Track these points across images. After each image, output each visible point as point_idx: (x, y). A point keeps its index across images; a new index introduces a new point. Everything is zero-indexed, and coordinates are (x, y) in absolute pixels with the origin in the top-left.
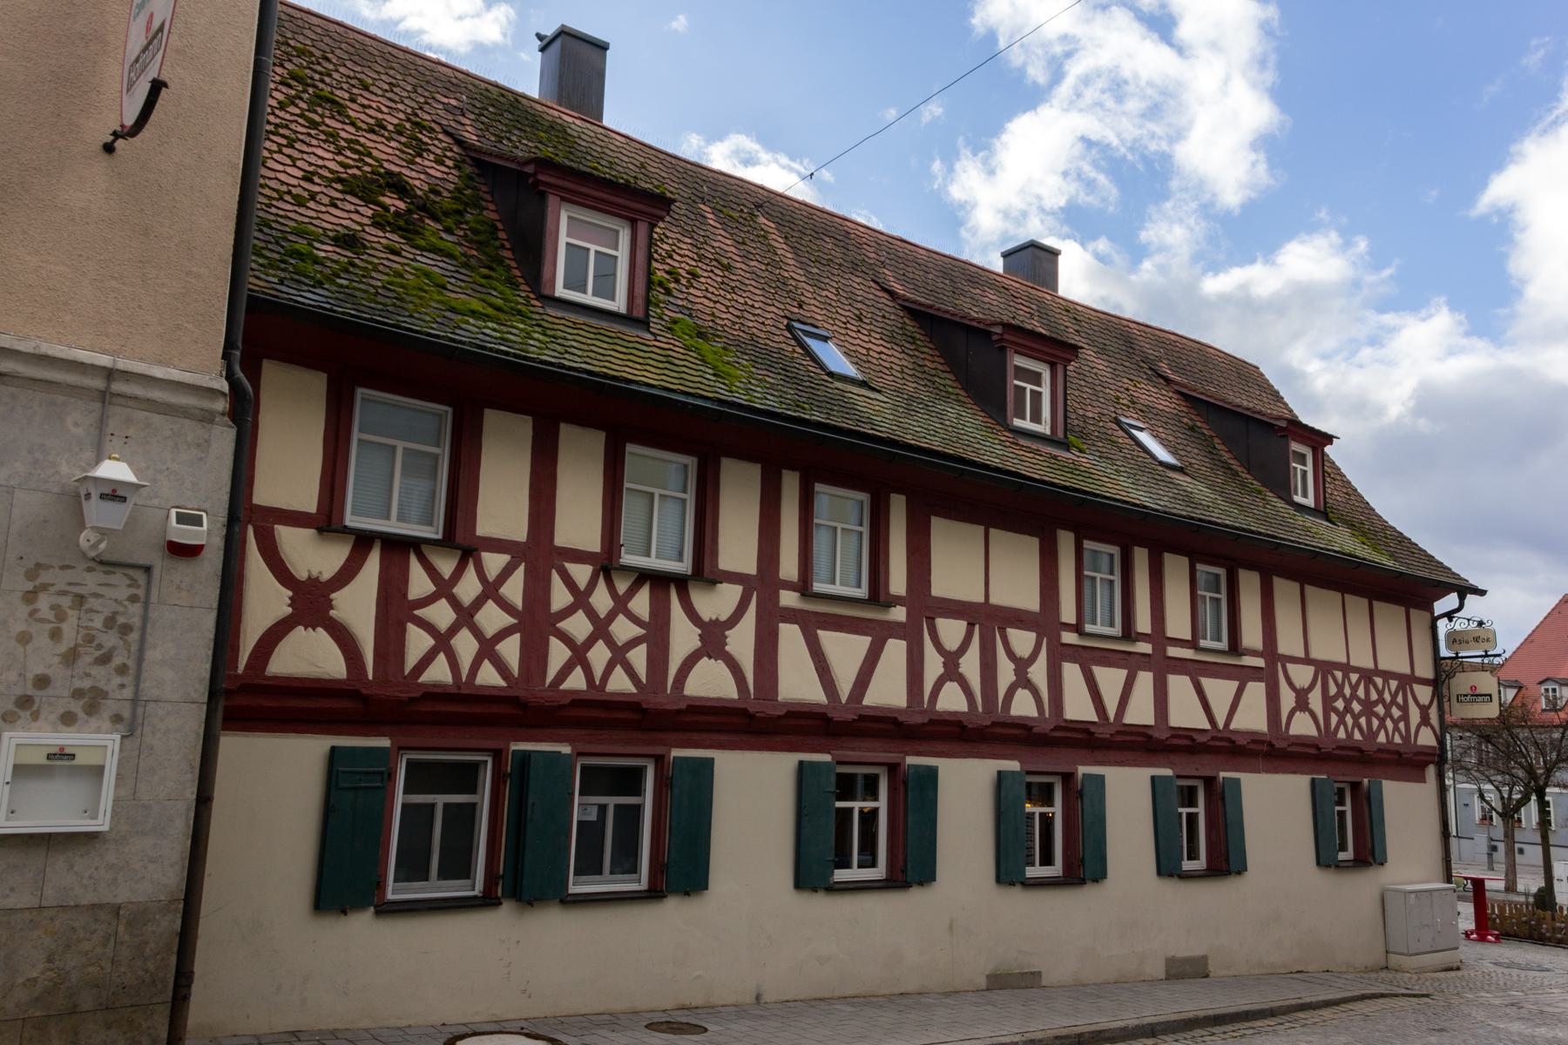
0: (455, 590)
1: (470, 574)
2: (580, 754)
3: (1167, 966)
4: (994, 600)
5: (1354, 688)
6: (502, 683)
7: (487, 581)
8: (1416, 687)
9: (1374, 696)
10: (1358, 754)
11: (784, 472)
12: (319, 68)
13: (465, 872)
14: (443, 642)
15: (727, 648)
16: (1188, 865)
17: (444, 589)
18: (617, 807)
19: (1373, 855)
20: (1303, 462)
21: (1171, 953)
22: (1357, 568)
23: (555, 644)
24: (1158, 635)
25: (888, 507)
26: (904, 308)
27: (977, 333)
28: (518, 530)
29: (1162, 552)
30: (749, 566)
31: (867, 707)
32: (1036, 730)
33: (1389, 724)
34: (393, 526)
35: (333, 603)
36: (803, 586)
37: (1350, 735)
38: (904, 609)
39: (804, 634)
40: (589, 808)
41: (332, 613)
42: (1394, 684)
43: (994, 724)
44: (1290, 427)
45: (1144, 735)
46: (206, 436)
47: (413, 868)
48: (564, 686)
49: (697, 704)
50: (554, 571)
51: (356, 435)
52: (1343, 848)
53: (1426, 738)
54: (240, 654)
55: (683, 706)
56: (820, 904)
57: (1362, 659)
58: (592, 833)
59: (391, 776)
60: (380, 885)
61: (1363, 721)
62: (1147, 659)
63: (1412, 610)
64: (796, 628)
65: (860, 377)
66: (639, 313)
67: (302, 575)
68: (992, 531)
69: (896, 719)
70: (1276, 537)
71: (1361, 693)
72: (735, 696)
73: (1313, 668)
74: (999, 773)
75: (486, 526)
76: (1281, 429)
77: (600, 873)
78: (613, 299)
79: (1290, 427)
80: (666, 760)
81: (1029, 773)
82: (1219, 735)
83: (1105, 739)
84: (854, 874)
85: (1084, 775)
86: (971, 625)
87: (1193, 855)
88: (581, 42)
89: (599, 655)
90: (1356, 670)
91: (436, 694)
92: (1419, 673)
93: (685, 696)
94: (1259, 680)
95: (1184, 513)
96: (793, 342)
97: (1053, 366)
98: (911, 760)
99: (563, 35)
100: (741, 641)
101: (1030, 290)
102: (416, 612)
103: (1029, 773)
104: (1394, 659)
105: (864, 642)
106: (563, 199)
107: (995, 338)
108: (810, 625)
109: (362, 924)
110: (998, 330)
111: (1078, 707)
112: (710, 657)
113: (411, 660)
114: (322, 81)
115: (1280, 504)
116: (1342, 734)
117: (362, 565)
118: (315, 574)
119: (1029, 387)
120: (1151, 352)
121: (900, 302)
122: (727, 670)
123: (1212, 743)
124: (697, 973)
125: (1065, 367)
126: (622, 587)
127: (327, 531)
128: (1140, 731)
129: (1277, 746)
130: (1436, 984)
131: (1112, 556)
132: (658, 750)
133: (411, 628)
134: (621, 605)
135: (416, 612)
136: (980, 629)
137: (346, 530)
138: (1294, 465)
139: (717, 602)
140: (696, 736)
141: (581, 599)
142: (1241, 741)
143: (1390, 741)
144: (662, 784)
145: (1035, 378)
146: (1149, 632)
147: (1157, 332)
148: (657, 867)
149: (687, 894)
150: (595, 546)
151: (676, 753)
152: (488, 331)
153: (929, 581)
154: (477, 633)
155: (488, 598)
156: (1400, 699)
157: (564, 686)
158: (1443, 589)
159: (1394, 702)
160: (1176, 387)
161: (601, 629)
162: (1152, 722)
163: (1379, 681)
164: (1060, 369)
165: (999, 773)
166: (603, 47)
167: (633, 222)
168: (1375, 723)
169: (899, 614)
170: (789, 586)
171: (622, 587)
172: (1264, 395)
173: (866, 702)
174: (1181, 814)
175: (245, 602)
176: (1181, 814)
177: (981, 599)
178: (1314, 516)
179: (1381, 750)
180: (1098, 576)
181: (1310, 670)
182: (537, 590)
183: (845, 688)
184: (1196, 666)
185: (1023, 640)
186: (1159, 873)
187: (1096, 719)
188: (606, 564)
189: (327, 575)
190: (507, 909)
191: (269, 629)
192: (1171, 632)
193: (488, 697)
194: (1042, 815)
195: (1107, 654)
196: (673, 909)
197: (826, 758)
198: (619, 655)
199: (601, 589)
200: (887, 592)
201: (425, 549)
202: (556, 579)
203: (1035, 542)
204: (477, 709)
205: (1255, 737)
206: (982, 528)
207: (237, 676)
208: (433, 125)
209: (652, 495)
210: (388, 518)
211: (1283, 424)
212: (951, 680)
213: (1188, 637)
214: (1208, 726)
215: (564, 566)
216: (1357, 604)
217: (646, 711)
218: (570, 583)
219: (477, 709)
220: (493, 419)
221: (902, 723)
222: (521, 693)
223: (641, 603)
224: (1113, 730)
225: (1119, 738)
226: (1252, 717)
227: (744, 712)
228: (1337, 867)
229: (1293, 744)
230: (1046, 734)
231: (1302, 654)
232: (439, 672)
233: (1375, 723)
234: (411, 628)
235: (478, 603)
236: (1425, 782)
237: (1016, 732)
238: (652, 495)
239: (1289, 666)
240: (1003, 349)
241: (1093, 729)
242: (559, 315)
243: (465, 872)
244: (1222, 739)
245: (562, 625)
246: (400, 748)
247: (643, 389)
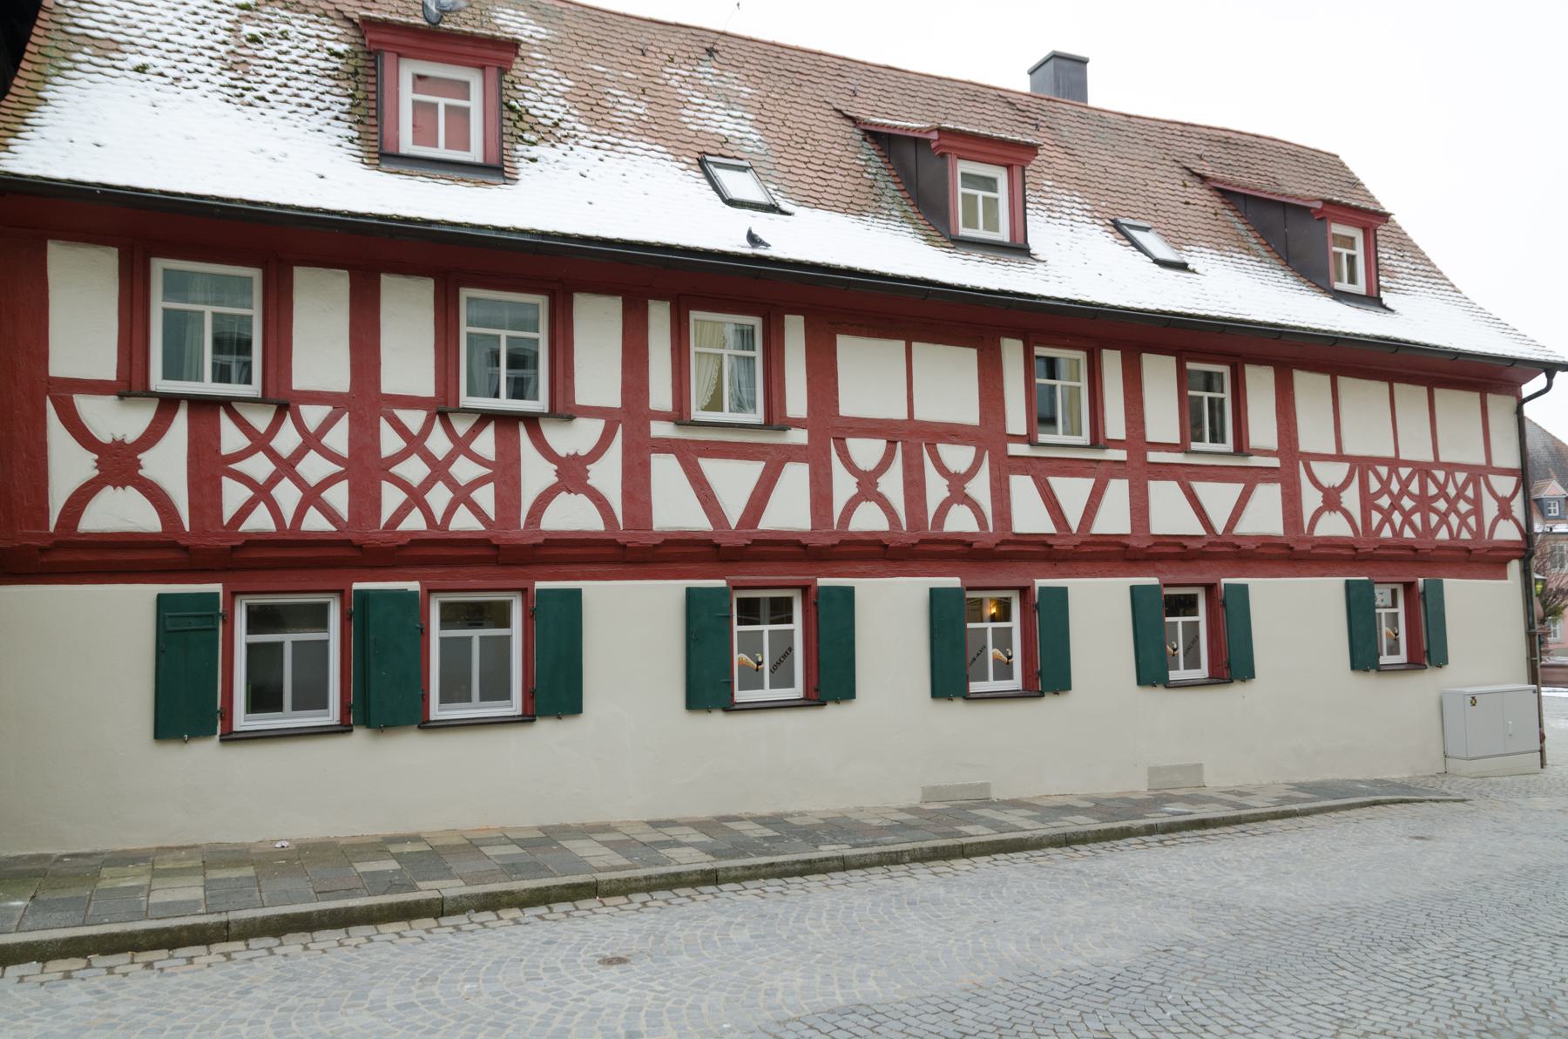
0: (272, 444)
1: (288, 426)
2: (736, 588)
6: (332, 528)
8: (1493, 478)
10: (1411, 553)
11: (650, 302)
13: (505, 694)
15: (589, 482)
17: (260, 443)
18: (482, 638)
22: (1279, 337)
24: (1136, 438)
27: (917, 142)
28: (338, 379)
30: (613, 399)
31: (763, 531)
35: (141, 463)
36: (680, 416)
37: (1397, 533)
41: (141, 472)
43: (922, 541)
44: (1326, 209)
47: (455, 691)
49: (594, 537)
50: (382, 419)
51: (693, 349)
53: (1507, 532)
54: (51, 514)
55: (540, 540)
56: (1157, 695)
60: (227, 715)
62: (1122, 467)
63: (1395, 384)
66: (493, 161)
68: (915, 345)
71: (1414, 487)
74: (932, 590)
75: (301, 380)
76: (1319, 211)
77: (469, 699)
78: (467, 148)
80: (529, 593)
82: (1218, 541)
85: (1040, 588)
86: (892, 443)
89: (439, 497)
90: (1407, 463)
91: (258, 541)
92: (1498, 462)
93: (541, 531)
98: (823, 582)
105: (1236, 489)
107: (933, 145)
108: (689, 455)
109: (206, 751)
111: (1030, 517)
113: (229, 511)
116: (1387, 533)
117: (169, 426)
118: (119, 437)
119: (981, 194)
121: (863, 127)
123: (1208, 549)
126: (462, 427)
127: (128, 396)
132: (521, 583)
133: (226, 481)
134: (462, 446)
136: (990, 456)
138: (1335, 249)
140: (564, 569)
141: (415, 444)
143: (1397, 533)
144: (529, 616)
148: (528, 695)
155: (310, 449)
156: (1470, 492)
162: (1128, 531)
163: (1440, 475)
165: (932, 590)
168: (1434, 519)
170: (661, 416)
171: (462, 427)
177: (904, 415)
179: (1441, 547)
180: (725, 352)
182: (365, 439)
183: (1074, 521)
185: (958, 457)
188: (442, 409)
190: (360, 736)
191: (77, 490)
193: (317, 542)
195: (1066, 464)
198: (462, 495)
199: (438, 433)
201: (236, 406)
203: (972, 353)
204: (590, 551)
205: (1266, 542)
207: (51, 535)
210: (497, 395)
211: (1319, 205)
212: (867, 500)
213: (1177, 440)
214: (1201, 531)
217: (497, 546)
219: (590, 551)
221: (806, 546)
222: (352, 535)
223: (486, 443)
224: (1078, 541)
227: (612, 543)
228: (1379, 670)
229: (1319, 546)
230: (991, 549)
231: (1333, 451)
232: (260, 521)
233: (1434, 519)
234: (226, 481)
237: (954, 548)
239: (1314, 465)
240: (943, 155)
241: (1050, 541)
243: (505, 694)
244: (1222, 545)
245: (396, 470)
246: (430, 591)
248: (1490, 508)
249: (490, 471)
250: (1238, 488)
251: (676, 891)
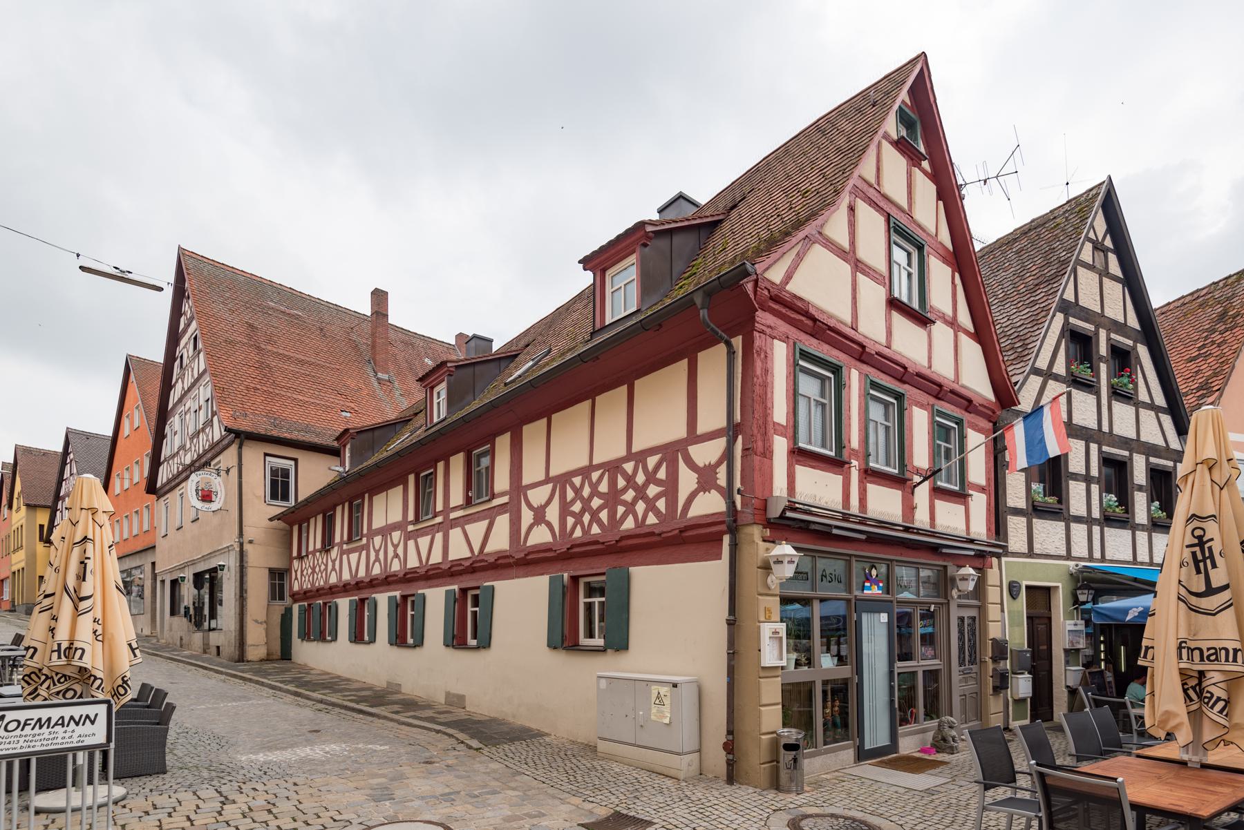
32: (219, 607)
37: (586, 531)
87: (590, 635)
99: (682, 200)
128: (436, 567)
143: (640, 524)
195: (425, 530)
224: (425, 569)
229: (529, 553)
248: (687, 480)
249: (619, 475)
250: (485, 523)
251: (56, 524)
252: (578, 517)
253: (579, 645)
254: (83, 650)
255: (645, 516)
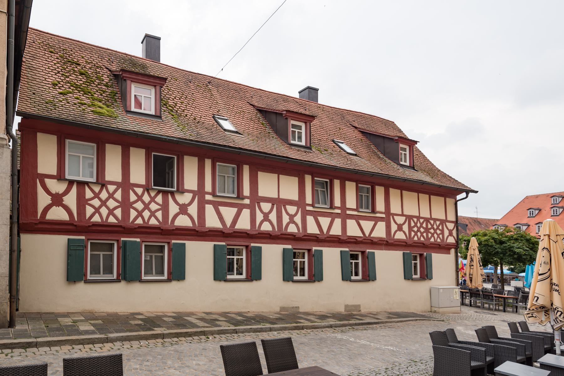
1: (104, 191)
3: (345, 307)
4: (281, 197)
5: (421, 224)
6: (116, 222)
7: (110, 193)
8: (447, 224)
9: (430, 226)
12: (69, 54)
14: (97, 210)
15: (188, 212)
16: (414, 276)
17: (97, 196)
19: (427, 277)
20: (405, 150)
21: (346, 304)
23: (132, 211)
25: (243, 169)
26: (257, 110)
27: (278, 114)
28: (119, 179)
29: (345, 181)
32: (296, 236)
33: (436, 236)
34: (81, 178)
36: (213, 194)
37: (419, 239)
38: (249, 200)
39: (214, 208)
40: (147, 256)
41: (63, 202)
42: (438, 223)
43: (281, 234)
45: (316, 237)
46: (2, 151)
48: (136, 223)
50: (131, 190)
52: (416, 273)
53: (451, 240)
55: (174, 228)
57: (425, 214)
58: (148, 263)
59: (86, 247)
60: (85, 275)
61: (425, 234)
62: (339, 215)
64: (211, 206)
65: (355, 153)
66: (158, 114)
67: (54, 192)
68: (280, 176)
69: (246, 232)
70: (389, 175)
71: (424, 225)
72: (192, 226)
73: (405, 217)
79: (399, 139)
81: (294, 249)
82: (367, 238)
83: (322, 239)
84: (235, 277)
86: (273, 205)
88: (154, 39)
89: (146, 214)
90: (422, 218)
91: (95, 225)
92: (449, 219)
94: (383, 221)
95: (352, 168)
96: (214, 121)
97: (306, 123)
98: (252, 245)
100: (193, 210)
101: (306, 102)
102: (89, 202)
103: (294, 249)
104: (438, 213)
105: (235, 210)
106: (132, 81)
108: (216, 205)
109: (81, 287)
110: (285, 112)
111: (312, 229)
112: (183, 214)
113: (88, 216)
114: (69, 57)
115: (395, 166)
116: (416, 238)
118: (57, 192)
119: (297, 131)
120: (351, 119)
121: (256, 108)
122: (188, 218)
123: (364, 241)
124: (183, 302)
125: (310, 123)
129: (389, 242)
130: (447, 318)
131: (233, 168)
134: (153, 200)
135: (89, 202)
137: (67, 180)
138: (401, 152)
139: (184, 199)
140: (180, 237)
141: (140, 198)
142: (375, 240)
143: (419, 239)
144: (170, 250)
145: (300, 128)
146: (340, 206)
147: (354, 113)
148: (169, 273)
149: (178, 280)
150: (143, 183)
151: (173, 241)
152: (186, 134)
153: (258, 192)
154: (107, 208)
156: (440, 227)
157: (136, 223)
158: (460, 191)
159: (438, 228)
160: (359, 130)
161: (146, 206)
163: (432, 222)
164: (308, 124)
166: (159, 39)
167: (155, 86)
169: (247, 201)
172: (395, 131)
173: (236, 227)
174: (352, 263)
175: (38, 200)
176: (352, 263)
177: (277, 197)
178: (409, 168)
180: (363, 194)
181: (404, 218)
182: (125, 196)
184: (358, 217)
185: (292, 209)
186: (343, 280)
187: (319, 233)
189: (61, 192)
190: (123, 283)
192: (348, 206)
194: (301, 262)
196: (174, 284)
197: (224, 244)
198: (153, 214)
199: (146, 195)
200: (243, 195)
201: (90, 184)
202: (131, 192)
203: (296, 179)
205: (381, 239)
206: (399, 191)
208: (102, 66)
209: (225, 176)
211: (397, 138)
213: (355, 208)
215: (134, 189)
216: (424, 198)
218: (136, 194)
220: (108, 147)
223: (159, 199)
224: (326, 236)
225: (328, 239)
226: (380, 232)
227: (195, 230)
229: (396, 241)
231: (401, 213)
233: (430, 235)
234: (87, 207)
235: (107, 199)
236: (450, 254)
238: (225, 176)
239: (395, 217)
240: (287, 118)
241: (318, 236)
242: (132, 116)
243: (162, 273)
244: (368, 240)
247: (152, 135)
252: (416, 234)
253: (142, 280)
254: (538, 298)
255: (414, 237)
